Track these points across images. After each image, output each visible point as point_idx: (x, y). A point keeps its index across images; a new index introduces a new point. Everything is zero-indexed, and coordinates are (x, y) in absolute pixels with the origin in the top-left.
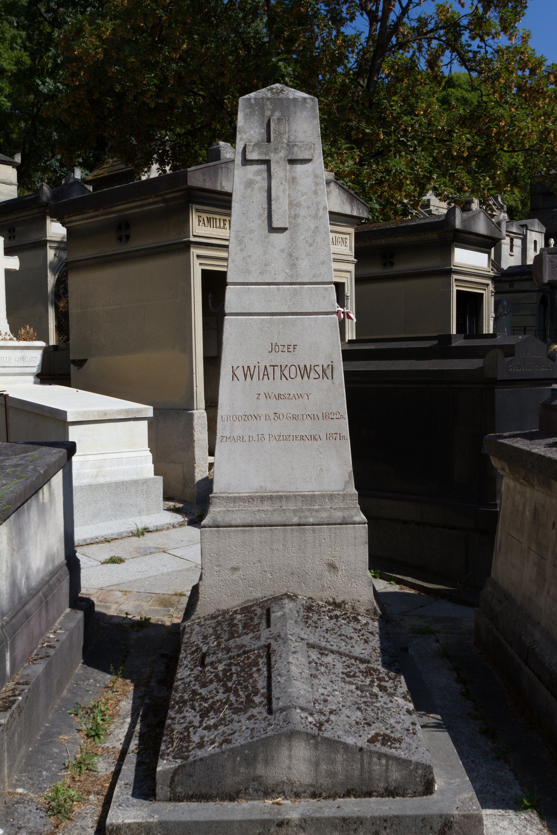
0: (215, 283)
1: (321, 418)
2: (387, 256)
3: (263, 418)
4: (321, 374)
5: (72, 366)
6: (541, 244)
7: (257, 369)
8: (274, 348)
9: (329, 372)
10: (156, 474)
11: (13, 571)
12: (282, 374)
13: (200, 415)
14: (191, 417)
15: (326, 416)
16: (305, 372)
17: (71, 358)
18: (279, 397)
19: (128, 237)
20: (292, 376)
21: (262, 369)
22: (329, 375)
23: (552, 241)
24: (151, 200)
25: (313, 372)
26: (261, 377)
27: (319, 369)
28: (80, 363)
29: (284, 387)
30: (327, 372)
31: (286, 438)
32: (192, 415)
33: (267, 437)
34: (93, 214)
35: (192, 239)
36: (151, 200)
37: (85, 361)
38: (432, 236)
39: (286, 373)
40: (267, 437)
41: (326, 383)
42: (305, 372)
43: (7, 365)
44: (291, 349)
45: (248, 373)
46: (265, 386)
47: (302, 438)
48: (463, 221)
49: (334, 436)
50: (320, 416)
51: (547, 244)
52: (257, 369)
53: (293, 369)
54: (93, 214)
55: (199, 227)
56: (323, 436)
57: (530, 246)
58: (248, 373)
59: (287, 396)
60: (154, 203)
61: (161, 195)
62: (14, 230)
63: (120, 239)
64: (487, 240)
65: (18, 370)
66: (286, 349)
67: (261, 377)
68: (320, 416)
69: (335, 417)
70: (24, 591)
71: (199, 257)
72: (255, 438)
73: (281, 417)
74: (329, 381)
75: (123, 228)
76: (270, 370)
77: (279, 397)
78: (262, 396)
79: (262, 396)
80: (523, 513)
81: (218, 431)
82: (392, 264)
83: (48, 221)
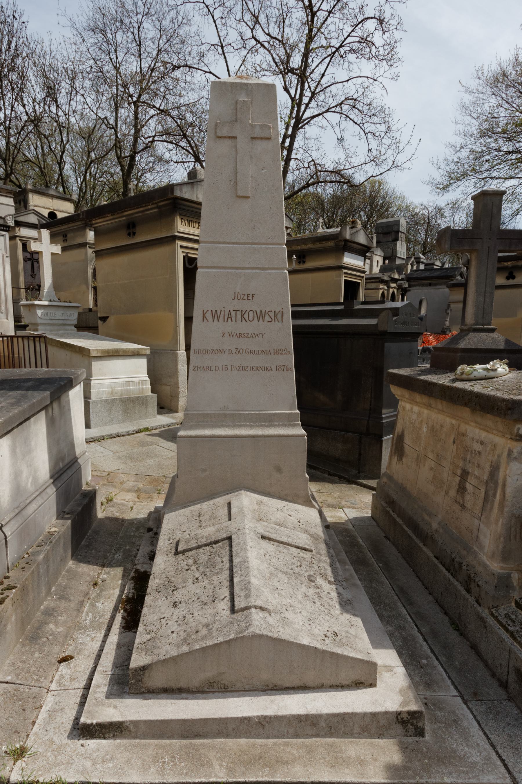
0: (191, 268)
1: (272, 354)
2: (302, 256)
3: (227, 352)
4: (273, 318)
5: (99, 321)
6: (381, 263)
7: (222, 313)
8: (236, 296)
9: (279, 316)
10: (152, 392)
11: (17, 475)
12: (242, 316)
13: (182, 353)
14: (176, 356)
15: (276, 352)
16: (261, 316)
17: (99, 315)
18: (240, 335)
19: (134, 234)
20: (251, 319)
21: (227, 313)
22: (280, 319)
23: (387, 261)
24: (149, 207)
25: (267, 316)
26: (226, 320)
27: (272, 314)
28: (104, 319)
29: (243, 327)
30: (278, 316)
31: (244, 369)
32: (177, 353)
33: (230, 368)
34: (111, 217)
35: (177, 234)
36: (149, 207)
37: (107, 317)
38: (330, 244)
39: (246, 316)
40: (230, 368)
41: (277, 325)
42: (261, 316)
43: (53, 318)
44: (250, 298)
45: (216, 316)
46: (230, 326)
47: (257, 369)
48: (351, 234)
49: (282, 367)
50: (272, 351)
51: (384, 263)
52: (222, 313)
53: (251, 314)
54: (111, 217)
55: (182, 227)
56: (274, 368)
57: (375, 264)
58: (216, 316)
59: (246, 335)
60: (152, 209)
61: (156, 203)
62: (66, 236)
63: (129, 234)
64: (364, 248)
65: (61, 322)
66: (246, 297)
67: (226, 320)
68: (272, 351)
69: (284, 352)
70: (30, 487)
71: (182, 247)
72: (221, 368)
73: (241, 352)
74: (279, 324)
75: (131, 227)
76: (233, 313)
77: (240, 335)
78: (227, 335)
79: (227, 335)
80: (420, 428)
81: (328, 487)
82: (304, 262)
83: (88, 230)
